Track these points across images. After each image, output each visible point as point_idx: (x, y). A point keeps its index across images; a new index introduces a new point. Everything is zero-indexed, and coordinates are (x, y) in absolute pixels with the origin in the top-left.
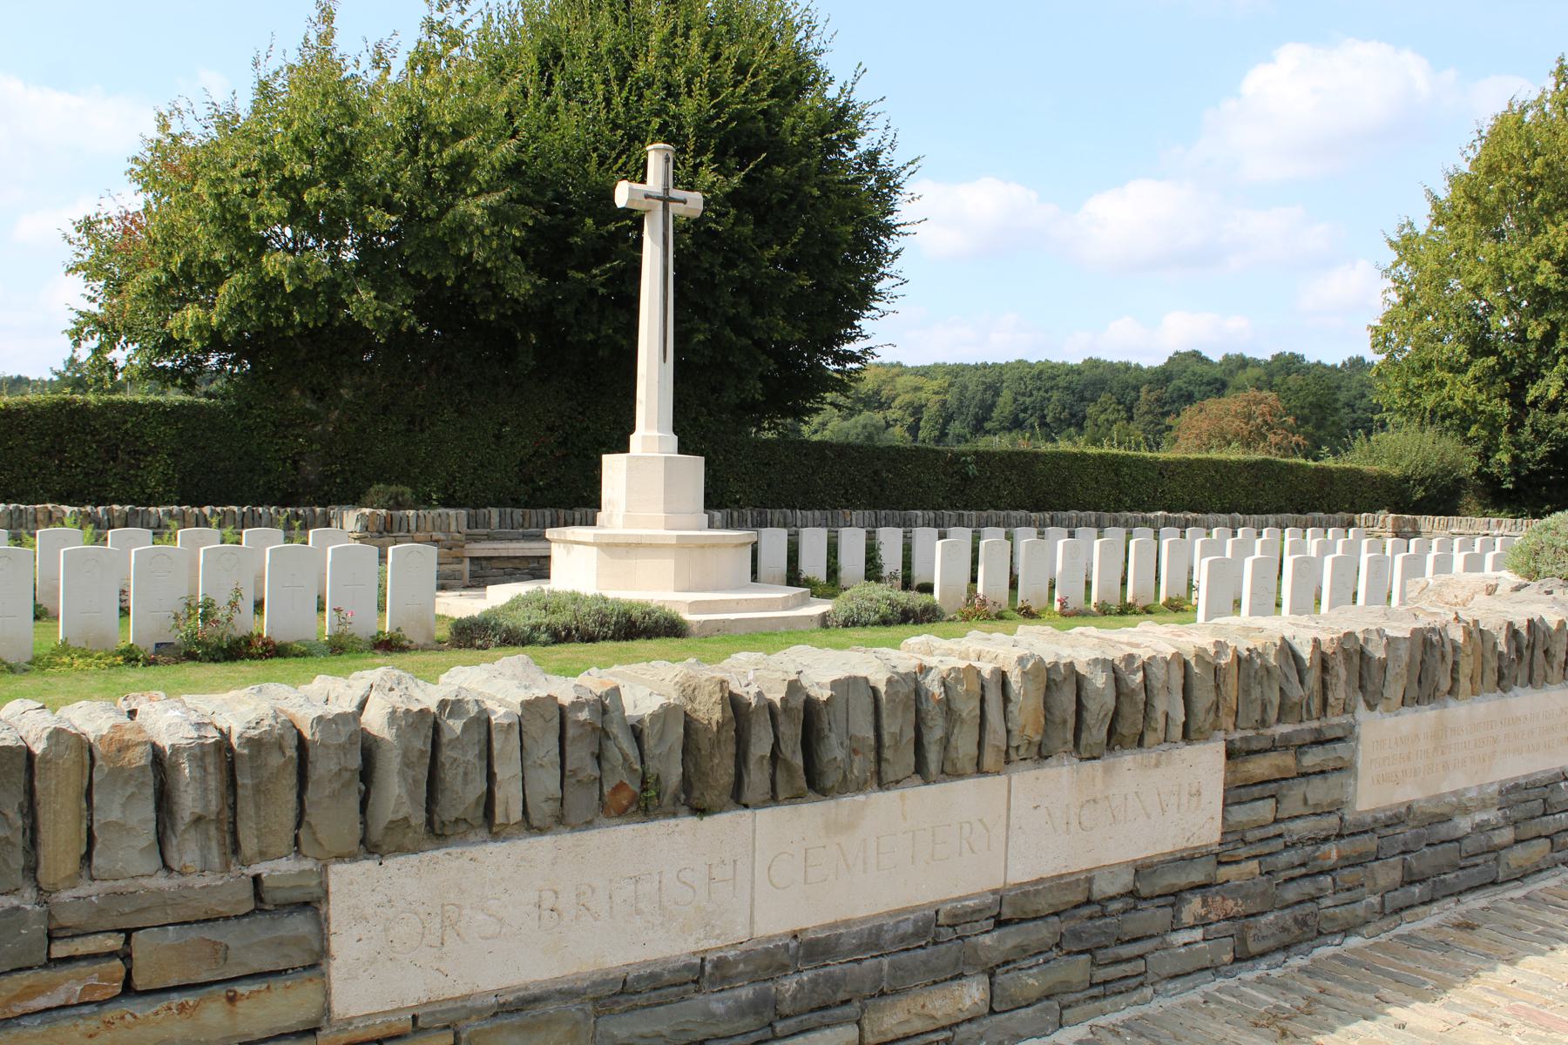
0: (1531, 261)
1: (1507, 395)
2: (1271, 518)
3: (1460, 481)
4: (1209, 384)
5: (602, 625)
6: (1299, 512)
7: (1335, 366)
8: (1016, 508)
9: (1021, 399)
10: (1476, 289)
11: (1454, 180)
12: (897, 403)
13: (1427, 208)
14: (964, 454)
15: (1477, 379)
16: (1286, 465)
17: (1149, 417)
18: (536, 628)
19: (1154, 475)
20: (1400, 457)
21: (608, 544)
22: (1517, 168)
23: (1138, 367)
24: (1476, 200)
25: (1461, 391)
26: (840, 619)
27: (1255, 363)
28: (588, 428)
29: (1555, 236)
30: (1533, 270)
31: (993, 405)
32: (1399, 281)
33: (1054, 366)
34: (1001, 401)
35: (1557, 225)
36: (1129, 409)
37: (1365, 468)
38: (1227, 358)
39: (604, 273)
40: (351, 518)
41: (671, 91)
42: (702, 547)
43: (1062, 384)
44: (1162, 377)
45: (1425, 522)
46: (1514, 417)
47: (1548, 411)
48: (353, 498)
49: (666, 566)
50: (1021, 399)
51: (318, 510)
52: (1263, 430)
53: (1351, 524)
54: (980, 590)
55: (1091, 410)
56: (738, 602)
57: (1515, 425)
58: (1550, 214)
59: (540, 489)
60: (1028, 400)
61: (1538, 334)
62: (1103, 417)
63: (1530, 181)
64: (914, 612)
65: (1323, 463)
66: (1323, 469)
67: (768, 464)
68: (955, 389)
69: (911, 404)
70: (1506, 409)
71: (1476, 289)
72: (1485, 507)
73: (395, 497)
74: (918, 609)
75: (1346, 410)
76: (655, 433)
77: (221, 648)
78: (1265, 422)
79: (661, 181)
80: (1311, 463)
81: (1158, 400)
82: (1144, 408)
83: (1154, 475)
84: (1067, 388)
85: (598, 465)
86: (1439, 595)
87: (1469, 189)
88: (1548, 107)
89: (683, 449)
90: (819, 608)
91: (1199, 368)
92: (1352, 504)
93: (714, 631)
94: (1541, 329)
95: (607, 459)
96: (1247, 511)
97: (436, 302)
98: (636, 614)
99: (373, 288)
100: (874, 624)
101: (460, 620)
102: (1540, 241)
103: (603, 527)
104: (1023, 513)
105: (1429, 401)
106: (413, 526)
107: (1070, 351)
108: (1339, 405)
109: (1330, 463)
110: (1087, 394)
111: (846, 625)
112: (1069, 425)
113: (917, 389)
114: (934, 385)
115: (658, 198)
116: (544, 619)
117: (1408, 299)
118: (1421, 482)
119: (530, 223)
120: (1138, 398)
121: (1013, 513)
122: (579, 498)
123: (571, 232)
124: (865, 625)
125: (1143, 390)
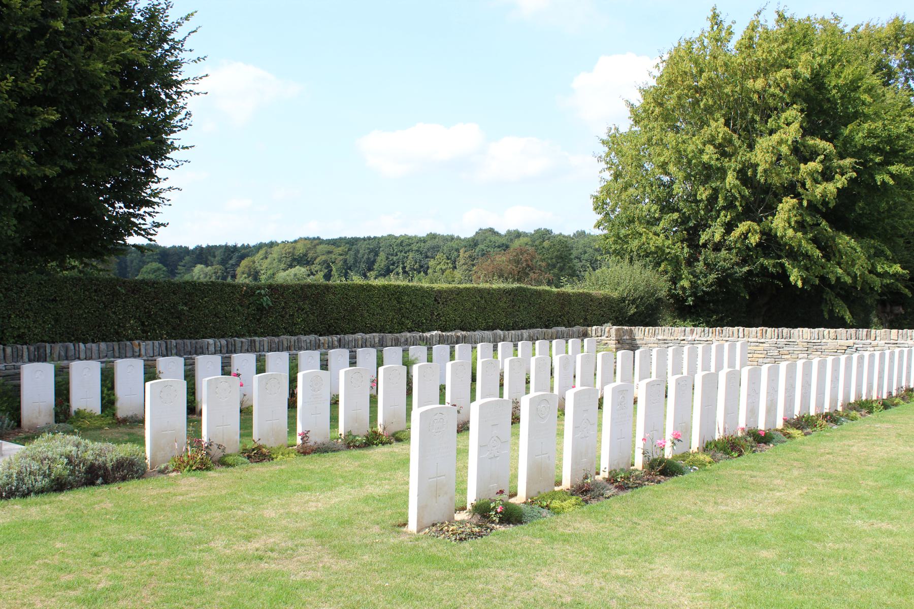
0: (700, 146)
1: (686, 240)
2: (525, 333)
3: (659, 300)
4: (499, 247)
6: (547, 327)
8: (306, 333)
9: (391, 258)
10: (663, 166)
11: (645, 92)
12: (317, 261)
13: (627, 112)
16: (536, 291)
17: (465, 267)
22: (689, 82)
24: (661, 105)
27: (525, 235)
29: (716, 128)
30: (701, 152)
31: (374, 262)
32: (610, 165)
33: (410, 238)
34: (379, 259)
35: (717, 121)
37: (594, 292)
43: (415, 248)
45: (640, 333)
46: (691, 255)
47: (714, 250)
50: (391, 258)
52: (527, 271)
53: (585, 335)
55: (432, 263)
57: (691, 261)
58: (712, 114)
60: (395, 258)
62: (439, 267)
63: (698, 90)
65: (563, 289)
66: (564, 293)
67: (54, 300)
68: (351, 252)
69: (325, 262)
70: (686, 251)
71: (663, 166)
72: (674, 318)
74: (109, 465)
75: (576, 261)
78: (528, 266)
80: (554, 290)
81: (470, 257)
82: (462, 262)
83: (430, 301)
84: (417, 251)
87: (656, 98)
88: (706, 41)
91: (493, 238)
92: (585, 319)
94: (707, 193)
96: (507, 328)
100: (42, 491)
102: (707, 132)
104: (312, 337)
105: (634, 244)
107: (418, 229)
108: (572, 257)
109: (568, 289)
110: (429, 254)
113: (330, 252)
114: (339, 250)
117: (617, 176)
118: (634, 301)
120: (459, 256)
121: (303, 338)
124: (25, 495)
125: (462, 251)
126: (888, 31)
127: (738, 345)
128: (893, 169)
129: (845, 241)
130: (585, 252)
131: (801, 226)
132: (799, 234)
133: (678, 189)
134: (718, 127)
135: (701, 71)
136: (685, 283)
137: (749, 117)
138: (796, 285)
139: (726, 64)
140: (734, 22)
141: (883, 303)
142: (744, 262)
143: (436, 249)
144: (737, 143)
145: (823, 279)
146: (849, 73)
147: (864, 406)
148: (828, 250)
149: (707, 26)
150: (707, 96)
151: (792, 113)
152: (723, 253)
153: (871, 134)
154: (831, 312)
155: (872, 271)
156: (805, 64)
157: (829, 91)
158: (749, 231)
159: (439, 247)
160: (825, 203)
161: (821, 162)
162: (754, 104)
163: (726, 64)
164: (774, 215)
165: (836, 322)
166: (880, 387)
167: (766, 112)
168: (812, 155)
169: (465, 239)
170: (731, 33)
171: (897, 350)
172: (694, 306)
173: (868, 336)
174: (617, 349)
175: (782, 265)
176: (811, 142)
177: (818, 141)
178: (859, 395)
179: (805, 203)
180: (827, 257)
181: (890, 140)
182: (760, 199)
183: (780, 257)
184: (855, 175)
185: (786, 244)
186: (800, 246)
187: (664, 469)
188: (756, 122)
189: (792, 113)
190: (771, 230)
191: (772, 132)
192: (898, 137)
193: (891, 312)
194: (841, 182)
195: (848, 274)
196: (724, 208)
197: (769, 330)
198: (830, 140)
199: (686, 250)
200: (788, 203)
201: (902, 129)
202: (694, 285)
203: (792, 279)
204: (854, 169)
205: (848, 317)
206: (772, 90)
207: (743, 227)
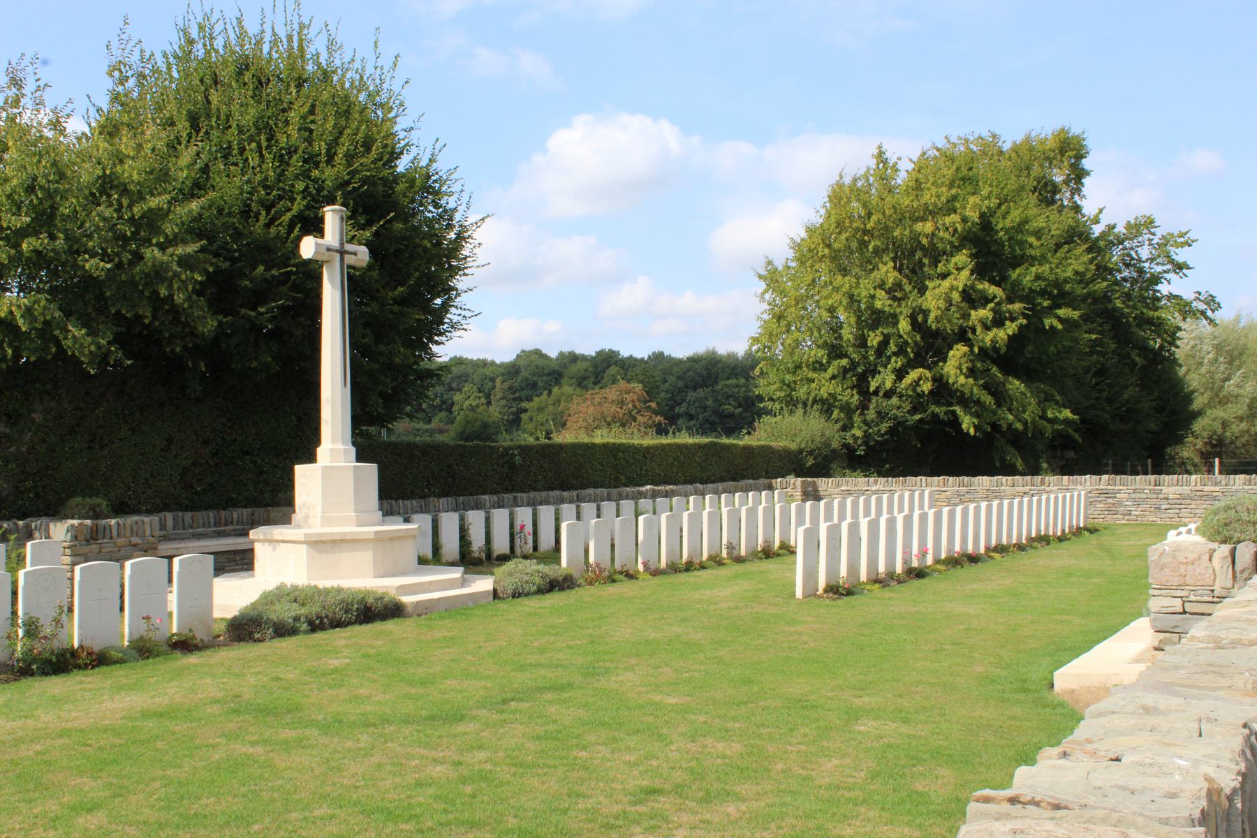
3: (834, 451)
4: (549, 374)
5: (346, 612)
7: (643, 359)
10: (831, 310)
14: (511, 448)
15: (833, 377)
17: (504, 402)
18: (296, 619)
19: (639, 457)
20: (795, 435)
21: (316, 542)
23: (493, 363)
24: (829, 246)
25: (825, 386)
26: (510, 592)
27: (584, 358)
28: (235, 440)
36: (488, 396)
38: (561, 354)
39: (270, 310)
40: (60, 531)
41: (311, 160)
42: (392, 539)
44: (512, 370)
45: (823, 484)
48: (54, 511)
49: (366, 557)
51: (21, 523)
54: (592, 559)
55: (458, 397)
56: (431, 583)
57: (864, 407)
59: (196, 493)
61: (875, 343)
62: (467, 403)
63: (865, 232)
64: (557, 581)
73: (92, 508)
76: (341, 447)
77: (50, 662)
79: (337, 237)
81: (510, 388)
82: (499, 395)
83: (639, 457)
85: (292, 471)
86: (1174, 557)
89: (360, 458)
90: (483, 584)
91: (540, 362)
92: (767, 472)
93: (425, 609)
95: (298, 469)
97: (131, 336)
98: (370, 600)
99: (83, 326)
101: (235, 618)
103: (299, 527)
106: (115, 534)
110: (454, 385)
111: (514, 596)
112: (441, 410)
115: (337, 251)
116: (296, 610)
118: (811, 453)
119: (211, 269)
120: (494, 387)
121: (551, 493)
122: (275, 501)
123: (242, 275)
125: (498, 380)
126: (1050, 144)
127: (926, 493)
128: (1061, 312)
129: (1015, 386)
130: (665, 381)
131: (972, 372)
132: (971, 380)
133: (847, 334)
134: (887, 271)
135: (869, 215)
136: (858, 433)
137: (917, 261)
138: (968, 433)
139: (894, 207)
140: (899, 159)
141: (1052, 448)
142: (914, 410)
143: (464, 378)
144: (908, 288)
145: (995, 426)
146: (1015, 215)
147: (1044, 540)
148: (1000, 395)
149: (873, 163)
150: (872, 235)
151: (962, 258)
152: (895, 400)
153: (1038, 277)
154: (1003, 460)
155: (1043, 417)
156: (972, 208)
157: (997, 232)
158: (920, 379)
159: (467, 375)
160: (995, 349)
161: (992, 310)
162: (923, 248)
163: (894, 207)
164: (945, 362)
165: (1010, 471)
166: (1055, 525)
167: (936, 255)
168: (985, 300)
169: (502, 365)
170: (897, 170)
171: (1068, 495)
172: (867, 454)
173: (1042, 483)
174: (804, 501)
175: (954, 413)
176: (980, 287)
177: (986, 285)
178: (1038, 530)
179: (976, 350)
180: (999, 405)
181: (1057, 284)
182: (931, 345)
183: (950, 405)
184: (1025, 322)
185: (957, 390)
186: (972, 393)
187: (918, 574)
188: (924, 265)
189: (962, 258)
190: (942, 376)
191: (944, 276)
192: (1066, 281)
193: (1062, 457)
194: (1011, 328)
195: (1020, 421)
196: (895, 354)
197: (951, 479)
198: (998, 284)
199: (856, 397)
200: (959, 351)
201: (1069, 273)
202: (867, 436)
203: (964, 426)
204: (1025, 316)
205: (1019, 464)
206: (941, 234)
207: (913, 375)
